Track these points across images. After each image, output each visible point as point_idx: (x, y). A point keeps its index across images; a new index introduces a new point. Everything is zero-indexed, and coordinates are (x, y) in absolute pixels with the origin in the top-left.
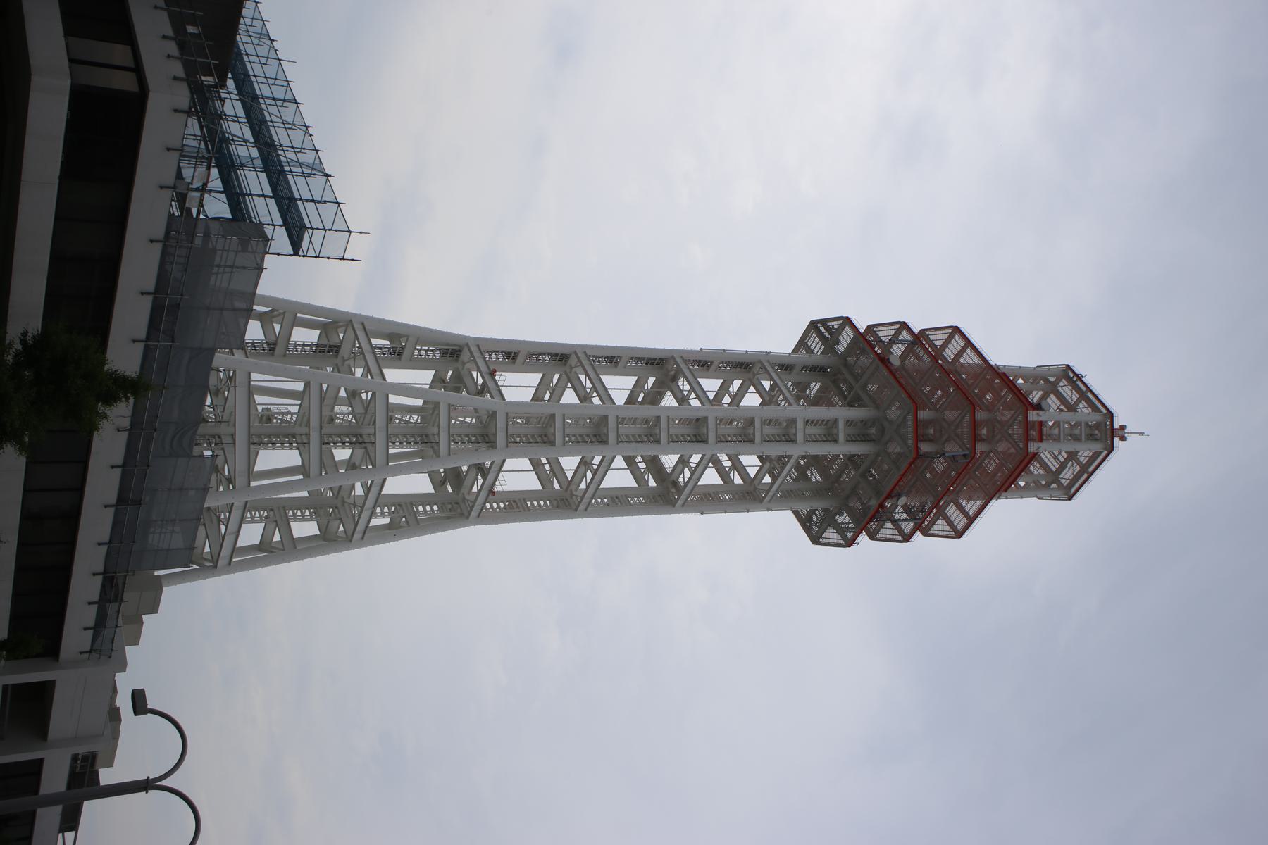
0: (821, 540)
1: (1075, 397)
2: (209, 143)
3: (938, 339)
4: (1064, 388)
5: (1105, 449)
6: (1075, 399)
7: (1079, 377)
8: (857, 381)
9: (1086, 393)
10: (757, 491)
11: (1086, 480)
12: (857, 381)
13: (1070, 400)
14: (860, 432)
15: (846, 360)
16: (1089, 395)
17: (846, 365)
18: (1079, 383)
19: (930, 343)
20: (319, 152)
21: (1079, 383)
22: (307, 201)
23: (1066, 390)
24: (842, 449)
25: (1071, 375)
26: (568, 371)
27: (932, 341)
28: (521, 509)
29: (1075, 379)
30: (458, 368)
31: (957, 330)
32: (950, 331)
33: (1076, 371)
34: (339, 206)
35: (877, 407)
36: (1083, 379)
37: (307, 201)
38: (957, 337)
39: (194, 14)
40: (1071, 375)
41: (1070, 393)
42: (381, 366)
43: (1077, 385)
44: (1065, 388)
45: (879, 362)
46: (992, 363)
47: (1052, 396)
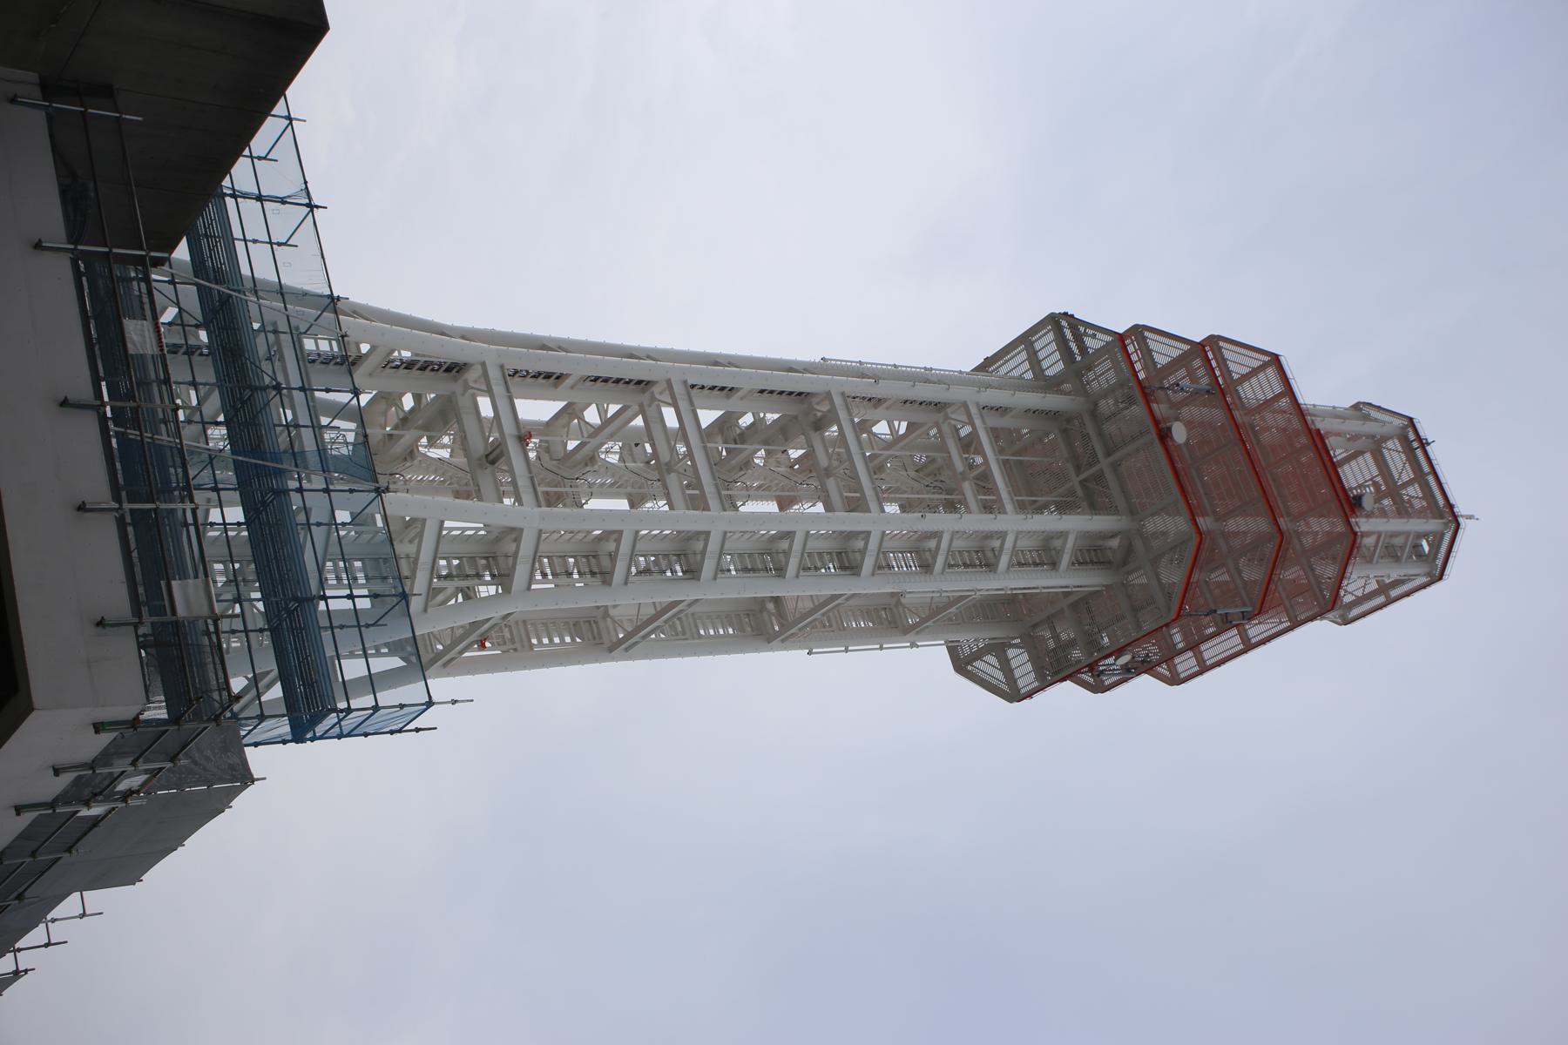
0: (969, 668)
1: (1408, 475)
2: (84, 279)
3: (1239, 364)
4: (1393, 453)
5: (1428, 574)
6: (1405, 478)
7: (1423, 444)
8: (1108, 454)
9: (1426, 473)
10: (900, 609)
11: (1380, 607)
12: (1108, 454)
13: (1396, 476)
14: (1092, 554)
15: (1096, 404)
16: (1431, 479)
17: (1094, 413)
18: (1419, 453)
19: (1216, 351)
20: (294, 122)
21: (1419, 453)
22: (246, 196)
23: (1396, 458)
24: (1065, 579)
25: (1412, 436)
26: (646, 403)
27: (1225, 360)
28: (518, 645)
29: (1415, 445)
30: (454, 393)
31: (1275, 360)
32: (1267, 359)
33: (1422, 434)
34: (291, 123)
35: (1132, 512)
36: (1428, 448)
37: (246, 196)
38: (1271, 372)
39: (155, 510)
40: (1412, 436)
41: (1400, 466)
42: (334, 508)
43: (1415, 456)
44: (1395, 454)
45: (1155, 436)
46: (1301, 401)
47: (1368, 456)
